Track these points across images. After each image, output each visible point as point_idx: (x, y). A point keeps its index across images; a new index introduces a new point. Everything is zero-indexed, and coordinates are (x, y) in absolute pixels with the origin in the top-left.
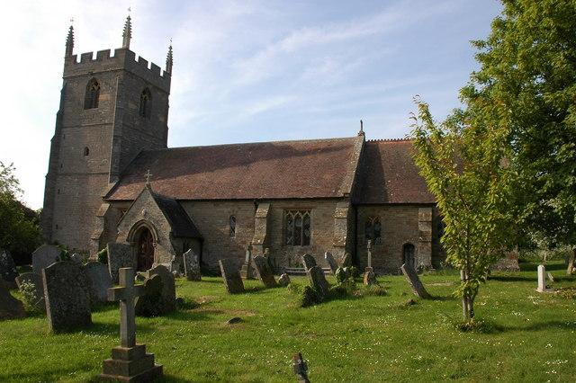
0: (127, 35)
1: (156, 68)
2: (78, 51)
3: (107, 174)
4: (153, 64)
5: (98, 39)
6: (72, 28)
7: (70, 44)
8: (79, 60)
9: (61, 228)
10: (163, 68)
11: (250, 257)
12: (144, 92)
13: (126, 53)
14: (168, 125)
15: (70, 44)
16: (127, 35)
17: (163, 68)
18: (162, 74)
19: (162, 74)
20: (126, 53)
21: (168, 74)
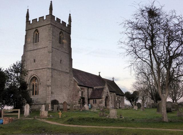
0: (51, 9)
1: (64, 23)
2: (31, 19)
3: (4, 116)
4: (62, 21)
5: (39, 12)
6: (28, 10)
7: (28, 16)
8: (31, 22)
9: (54, 93)
10: (67, 23)
11: (169, 129)
12: (60, 34)
13: (51, 16)
14: (72, 47)
15: (28, 16)
16: (51, 9)
17: (67, 23)
18: (67, 26)
19: (67, 26)
20: (51, 16)
21: (70, 26)
